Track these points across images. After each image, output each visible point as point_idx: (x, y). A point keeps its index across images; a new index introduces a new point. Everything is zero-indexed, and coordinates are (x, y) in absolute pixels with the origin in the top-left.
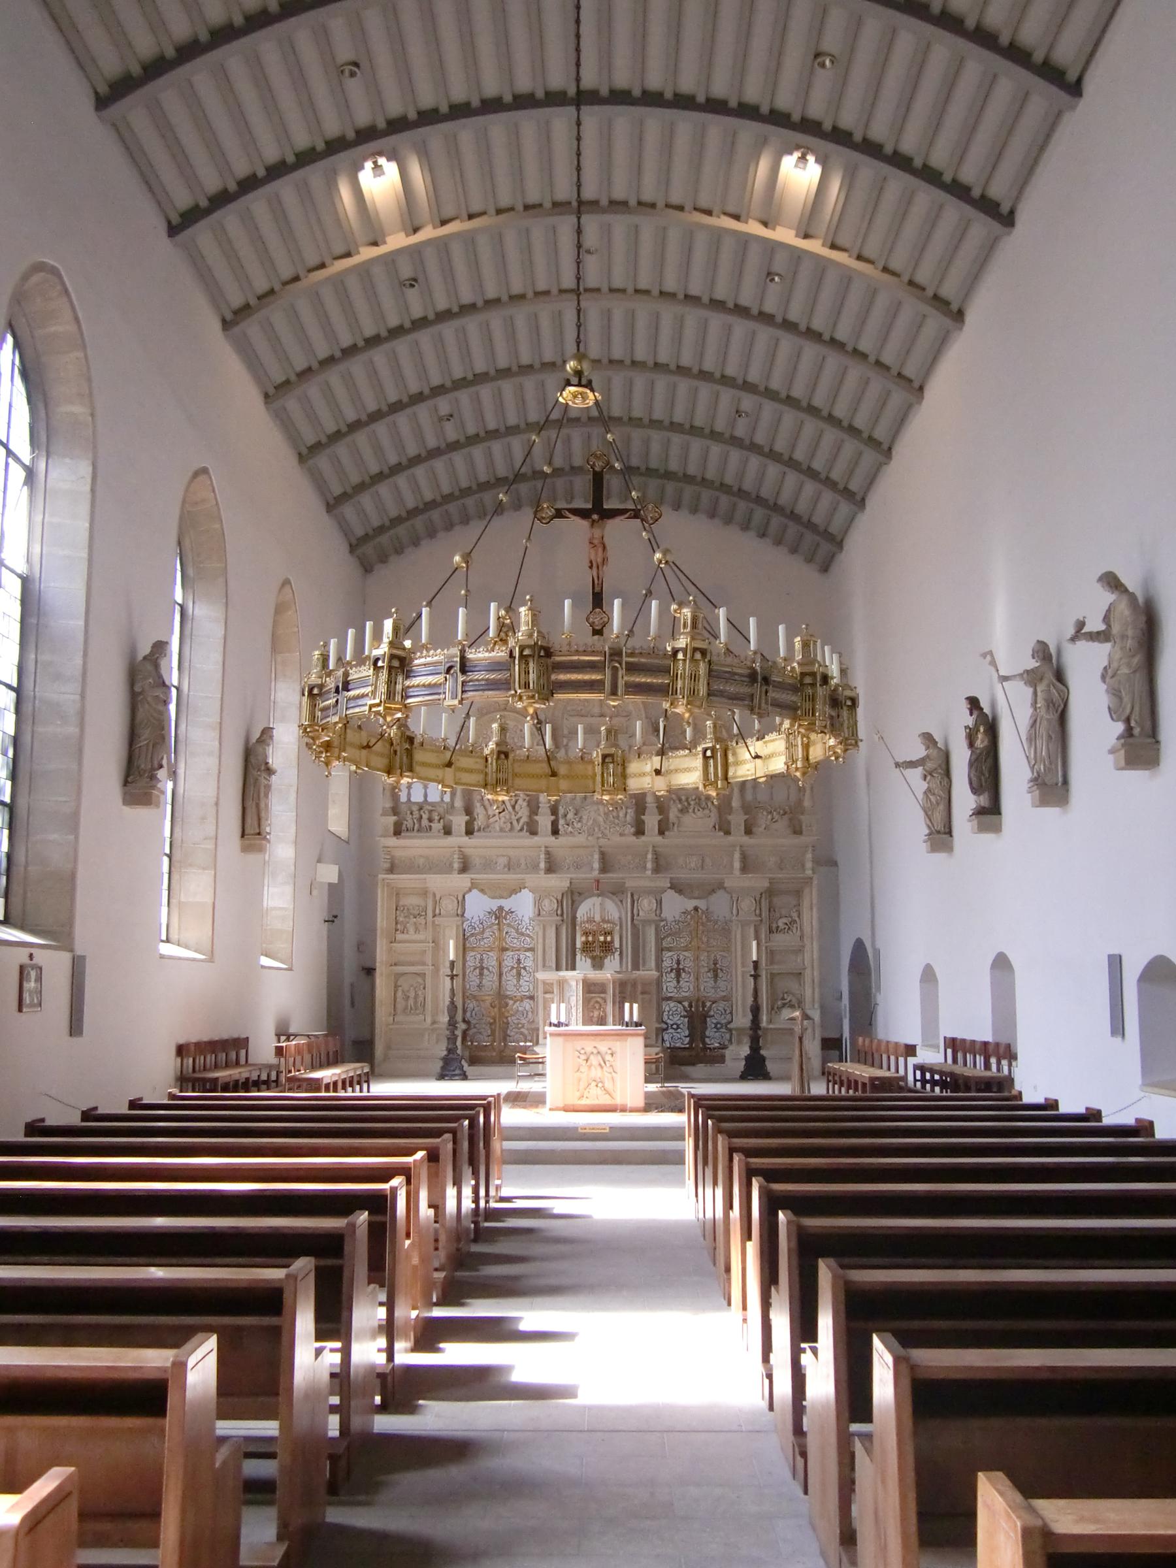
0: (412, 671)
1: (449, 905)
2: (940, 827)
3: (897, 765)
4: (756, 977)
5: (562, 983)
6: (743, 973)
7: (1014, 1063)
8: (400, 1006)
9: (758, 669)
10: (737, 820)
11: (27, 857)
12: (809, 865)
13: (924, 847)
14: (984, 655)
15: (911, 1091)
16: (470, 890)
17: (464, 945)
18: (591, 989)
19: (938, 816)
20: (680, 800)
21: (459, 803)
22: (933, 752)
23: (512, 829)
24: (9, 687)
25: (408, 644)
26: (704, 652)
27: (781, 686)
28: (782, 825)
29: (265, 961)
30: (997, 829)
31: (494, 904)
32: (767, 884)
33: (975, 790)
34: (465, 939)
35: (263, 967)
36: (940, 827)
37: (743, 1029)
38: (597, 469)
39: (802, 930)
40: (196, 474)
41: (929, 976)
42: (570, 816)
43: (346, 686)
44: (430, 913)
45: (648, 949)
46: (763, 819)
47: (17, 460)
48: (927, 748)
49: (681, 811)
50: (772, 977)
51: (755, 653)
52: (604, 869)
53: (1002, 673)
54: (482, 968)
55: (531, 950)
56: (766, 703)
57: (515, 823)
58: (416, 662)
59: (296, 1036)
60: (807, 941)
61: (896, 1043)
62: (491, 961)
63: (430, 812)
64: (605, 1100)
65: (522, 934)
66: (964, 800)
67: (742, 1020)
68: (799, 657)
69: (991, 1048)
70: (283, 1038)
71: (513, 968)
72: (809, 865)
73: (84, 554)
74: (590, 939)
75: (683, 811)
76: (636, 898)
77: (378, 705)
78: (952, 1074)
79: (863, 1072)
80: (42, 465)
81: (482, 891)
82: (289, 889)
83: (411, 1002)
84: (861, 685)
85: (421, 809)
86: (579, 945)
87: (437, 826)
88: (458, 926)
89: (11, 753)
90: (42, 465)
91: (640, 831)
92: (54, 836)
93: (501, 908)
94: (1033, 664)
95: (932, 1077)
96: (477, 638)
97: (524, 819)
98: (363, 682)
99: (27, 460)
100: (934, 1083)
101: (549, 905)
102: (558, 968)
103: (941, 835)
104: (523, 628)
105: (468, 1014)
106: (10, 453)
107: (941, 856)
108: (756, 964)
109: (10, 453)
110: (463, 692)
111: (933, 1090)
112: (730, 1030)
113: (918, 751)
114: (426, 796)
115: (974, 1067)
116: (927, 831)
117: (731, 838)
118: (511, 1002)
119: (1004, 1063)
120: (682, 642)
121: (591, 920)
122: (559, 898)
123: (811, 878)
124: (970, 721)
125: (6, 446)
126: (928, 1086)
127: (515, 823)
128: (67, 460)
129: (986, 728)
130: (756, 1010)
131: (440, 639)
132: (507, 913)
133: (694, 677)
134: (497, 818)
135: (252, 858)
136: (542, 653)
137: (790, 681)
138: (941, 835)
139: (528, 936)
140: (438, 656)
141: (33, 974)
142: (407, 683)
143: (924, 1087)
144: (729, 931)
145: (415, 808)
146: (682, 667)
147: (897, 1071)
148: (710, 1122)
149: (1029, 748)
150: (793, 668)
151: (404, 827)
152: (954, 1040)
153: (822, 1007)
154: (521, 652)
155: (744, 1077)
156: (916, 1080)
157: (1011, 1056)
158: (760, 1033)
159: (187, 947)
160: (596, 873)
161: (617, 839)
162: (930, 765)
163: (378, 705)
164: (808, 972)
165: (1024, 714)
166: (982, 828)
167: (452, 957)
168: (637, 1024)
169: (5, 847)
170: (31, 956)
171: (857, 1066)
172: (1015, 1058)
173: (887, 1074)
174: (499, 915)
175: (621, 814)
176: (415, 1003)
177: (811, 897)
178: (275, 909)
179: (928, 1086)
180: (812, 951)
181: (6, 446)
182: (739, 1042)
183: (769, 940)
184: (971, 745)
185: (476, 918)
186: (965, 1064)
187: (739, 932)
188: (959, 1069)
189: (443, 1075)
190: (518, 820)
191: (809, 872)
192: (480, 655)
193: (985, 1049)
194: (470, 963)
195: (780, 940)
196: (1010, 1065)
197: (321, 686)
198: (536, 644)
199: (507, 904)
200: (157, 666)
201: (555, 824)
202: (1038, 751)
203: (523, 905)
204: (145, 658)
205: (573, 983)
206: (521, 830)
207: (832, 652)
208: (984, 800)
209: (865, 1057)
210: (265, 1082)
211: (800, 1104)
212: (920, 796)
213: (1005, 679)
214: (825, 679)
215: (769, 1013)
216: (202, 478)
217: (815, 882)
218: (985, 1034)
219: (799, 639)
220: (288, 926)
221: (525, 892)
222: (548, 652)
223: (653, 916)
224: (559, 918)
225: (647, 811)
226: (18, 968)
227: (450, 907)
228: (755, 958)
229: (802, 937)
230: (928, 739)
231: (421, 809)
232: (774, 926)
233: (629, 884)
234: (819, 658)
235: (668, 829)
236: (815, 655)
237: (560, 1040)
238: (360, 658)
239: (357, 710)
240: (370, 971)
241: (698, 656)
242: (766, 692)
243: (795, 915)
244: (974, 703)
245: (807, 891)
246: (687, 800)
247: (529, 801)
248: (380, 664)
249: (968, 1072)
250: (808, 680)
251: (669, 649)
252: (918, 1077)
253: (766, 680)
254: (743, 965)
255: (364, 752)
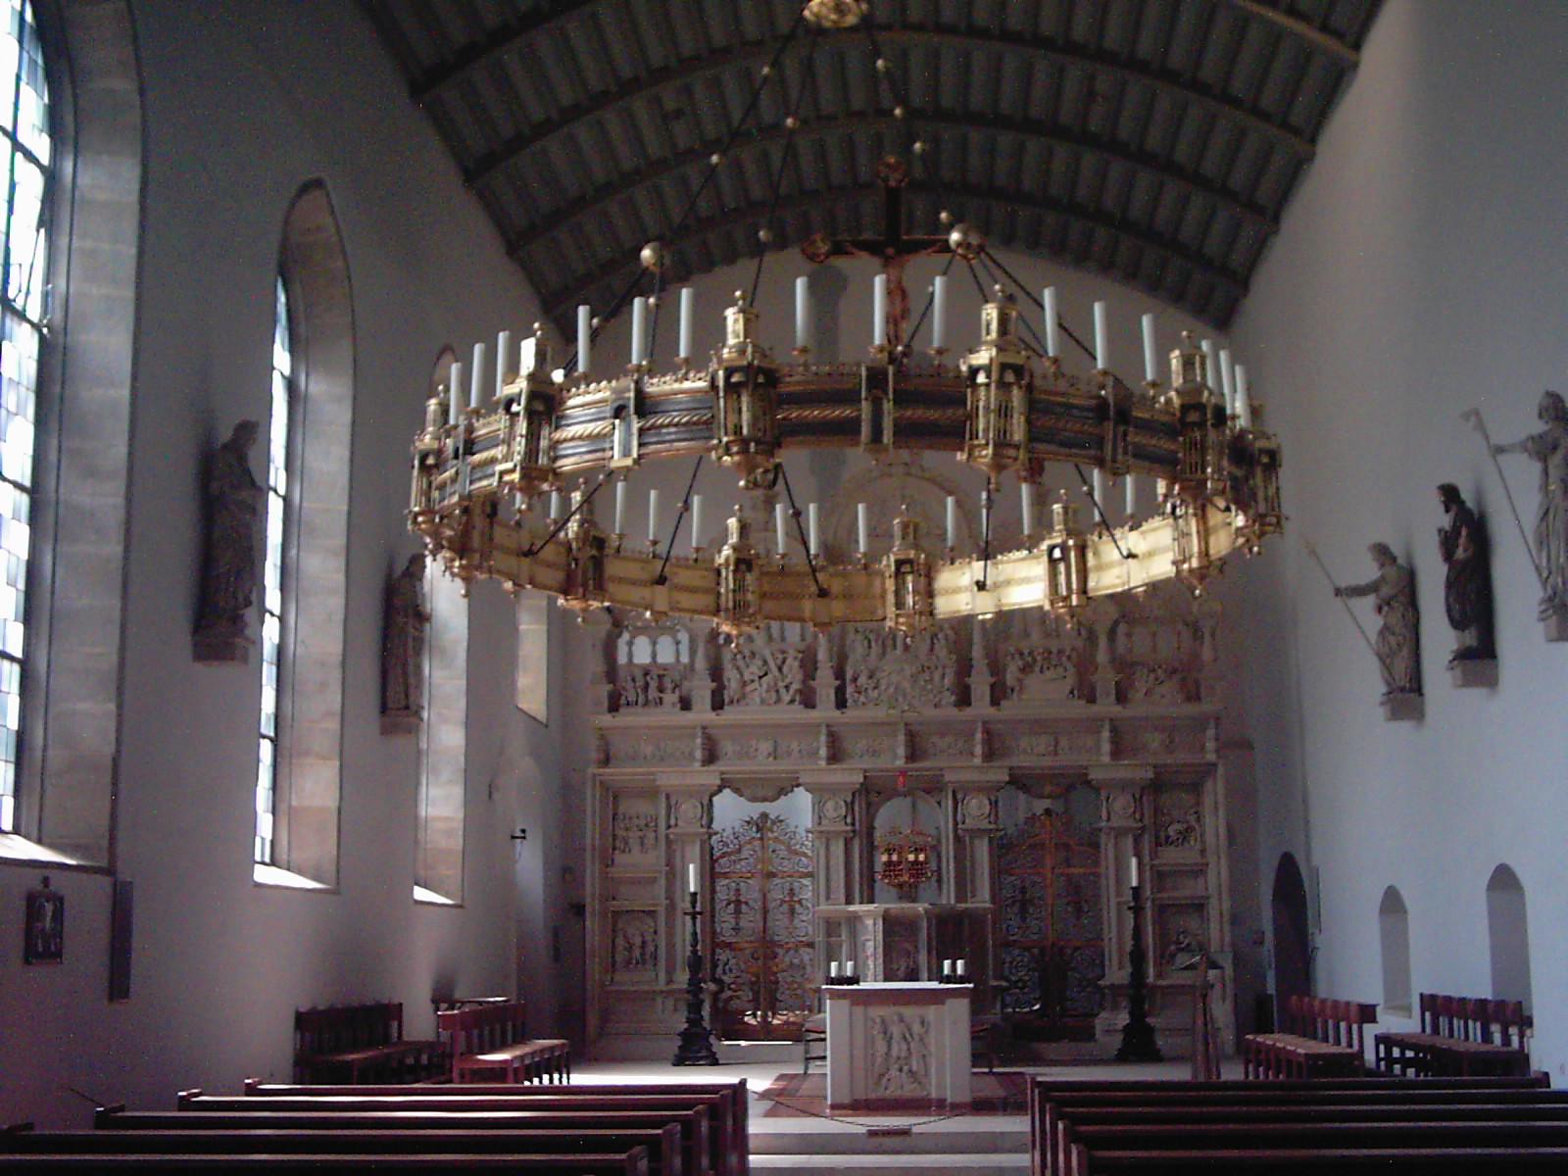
0: (563, 417)
1: (689, 810)
2: (1404, 682)
3: (1338, 592)
4: (1138, 910)
5: (854, 920)
6: (1119, 904)
7: (1528, 1032)
8: (619, 958)
9: (1111, 400)
10: (1105, 679)
11: (45, 739)
12: (1210, 745)
13: (1380, 713)
14: (1466, 416)
15: (1370, 1073)
16: (720, 790)
17: (712, 868)
18: (895, 929)
19: (1401, 666)
20: (1022, 654)
21: (701, 664)
22: (1391, 572)
23: (778, 700)
24: (17, 485)
25: (558, 376)
26: (1018, 370)
27: (1147, 426)
28: (1169, 688)
29: (420, 894)
30: (1490, 681)
31: (755, 809)
32: (1151, 775)
33: (1458, 623)
34: (713, 861)
35: (418, 902)
36: (1404, 682)
37: (1121, 987)
38: (892, 183)
39: (1203, 842)
40: (304, 189)
41: (1392, 903)
42: (862, 680)
43: (470, 446)
44: (662, 824)
45: (978, 873)
46: (1141, 685)
47: (30, 156)
48: (1382, 565)
49: (1023, 670)
50: (1162, 909)
51: (1105, 373)
52: (912, 757)
53: (1495, 440)
54: (738, 903)
55: (810, 875)
56: (1125, 453)
57: (783, 691)
58: (571, 403)
59: (463, 1003)
60: (1212, 859)
61: (1348, 1004)
62: (751, 891)
63: (660, 677)
64: (909, 1090)
65: (796, 853)
66: (1440, 638)
67: (1117, 974)
68: (1177, 381)
69: (1491, 1008)
70: (444, 1006)
71: (783, 901)
72: (1210, 745)
73: (129, 293)
74: (895, 858)
75: (1026, 669)
76: (959, 796)
77: (513, 471)
78: (1431, 1049)
79: (1301, 1046)
80: (68, 167)
81: (737, 791)
82: (457, 791)
83: (637, 953)
84: (1282, 433)
85: (646, 674)
86: (878, 868)
87: (670, 698)
88: (703, 843)
89: (21, 585)
90: (68, 167)
91: (964, 699)
92: (82, 706)
93: (764, 816)
94: (1538, 427)
95: (1403, 1053)
96: (661, 358)
97: (795, 686)
98: (493, 442)
99: (45, 159)
100: (1406, 1063)
101: (835, 808)
102: (849, 901)
103: (1406, 695)
104: (731, 341)
105: (719, 970)
106: (17, 146)
107: (1405, 727)
108: (1136, 891)
109: (17, 146)
110: (640, 445)
111: (1404, 1073)
112: (1100, 989)
113: (1368, 571)
114: (654, 656)
115: (1469, 1037)
116: (1384, 689)
117: (1094, 709)
118: (780, 951)
119: (1513, 1031)
120: (982, 357)
121: (894, 832)
122: (849, 800)
123: (1215, 765)
124: (1446, 521)
125: (12, 136)
126: (1397, 1068)
127: (783, 691)
128: (105, 158)
129: (1469, 538)
130: (1138, 957)
131: (608, 362)
132: (774, 823)
133: (1004, 412)
134: (756, 685)
135: (400, 741)
136: (761, 379)
137: (1165, 418)
138: (1406, 695)
139: (805, 855)
140: (602, 392)
141: (49, 907)
142: (557, 435)
143: (1389, 1068)
144: (1096, 846)
145: (639, 675)
146: (985, 397)
147: (1350, 1045)
148: (1061, 1126)
149: (1540, 550)
150: (1169, 401)
151: (623, 701)
152: (1433, 997)
153: (1236, 958)
154: (727, 378)
155: (1123, 1057)
156: (1379, 1059)
157: (1526, 1022)
158: (1145, 991)
159: (300, 872)
160: (900, 763)
161: (930, 713)
162: (1386, 590)
163: (513, 471)
164: (1214, 902)
165: (1530, 505)
166: (1469, 681)
167: (692, 890)
168: (962, 980)
169: (13, 722)
170: (46, 881)
171: (1289, 1038)
172: (1530, 1024)
173: (1334, 1050)
174: (762, 824)
175: (937, 677)
176: (643, 954)
177: (1215, 791)
178: (440, 819)
179: (1397, 1068)
180: (1218, 873)
181: (12, 136)
182: (1115, 1007)
183: (1154, 855)
184: (1448, 556)
185: (729, 831)
186: (1451, 1035)
187: (1110, 846)
188: (1443, 1041)
189: (681, 1061)
190: (787, 687)
191: (1211, 757)
192: (667, 388)
193: (1482, 1011)
194: (722, 895)
195: (1171, 856)
196: (1522, 1036)
197: (439, 453)
198: (750, 365)
199: (773, 809)
200: (242, 458)
201: (840, 692)
202: (1553, 557)
203: (799, 809)
204: (225, 447)
205: (869, 922)
206: (792, 701)
207: (1234, 361)
208: (1470, 638)
209: (1304, 1026)
210: (426, 1068)
211: (1202, 1093)
212: (1373, 637)
213: (1500, 450)
214: (1221, 416)
215: (1158, 964)
216: (317, 195)
217: (1221, 770)
218: (1480, 987)
219: (1177, 353)
220: (457, 843)
221: (800, 791)
222: (772, 377)
223: (985, 825)
224: (849, 828)
225: (974, 673)
226: (22, 905)
227: (691, 814)
228: (1134, 883)
229: (1203, 852)
230: (1383, 553)
231: (646, 674)
232: (1163, 838)
233: (948, 777)
234: (1210, 383)
235: (1005, 697)
236: (1204, 376)
237: (845, 1003)
238: (489, 404)
239: (485, 483)
240: (579, 910)
241: (1010, 377)
242: (1125, 435)
243: (1192, 819)
244: (1450, 495)
245: (1209, 785)
246: (1030, 653)
247: (802, 661)
248: (515, 408)
249: (1458, 1045)
250: (1193, 417)
251: (964, 368)
252: (1382, 1055)
253: (1123, 416)
254: (1118, 894)
255: (526, 561)
